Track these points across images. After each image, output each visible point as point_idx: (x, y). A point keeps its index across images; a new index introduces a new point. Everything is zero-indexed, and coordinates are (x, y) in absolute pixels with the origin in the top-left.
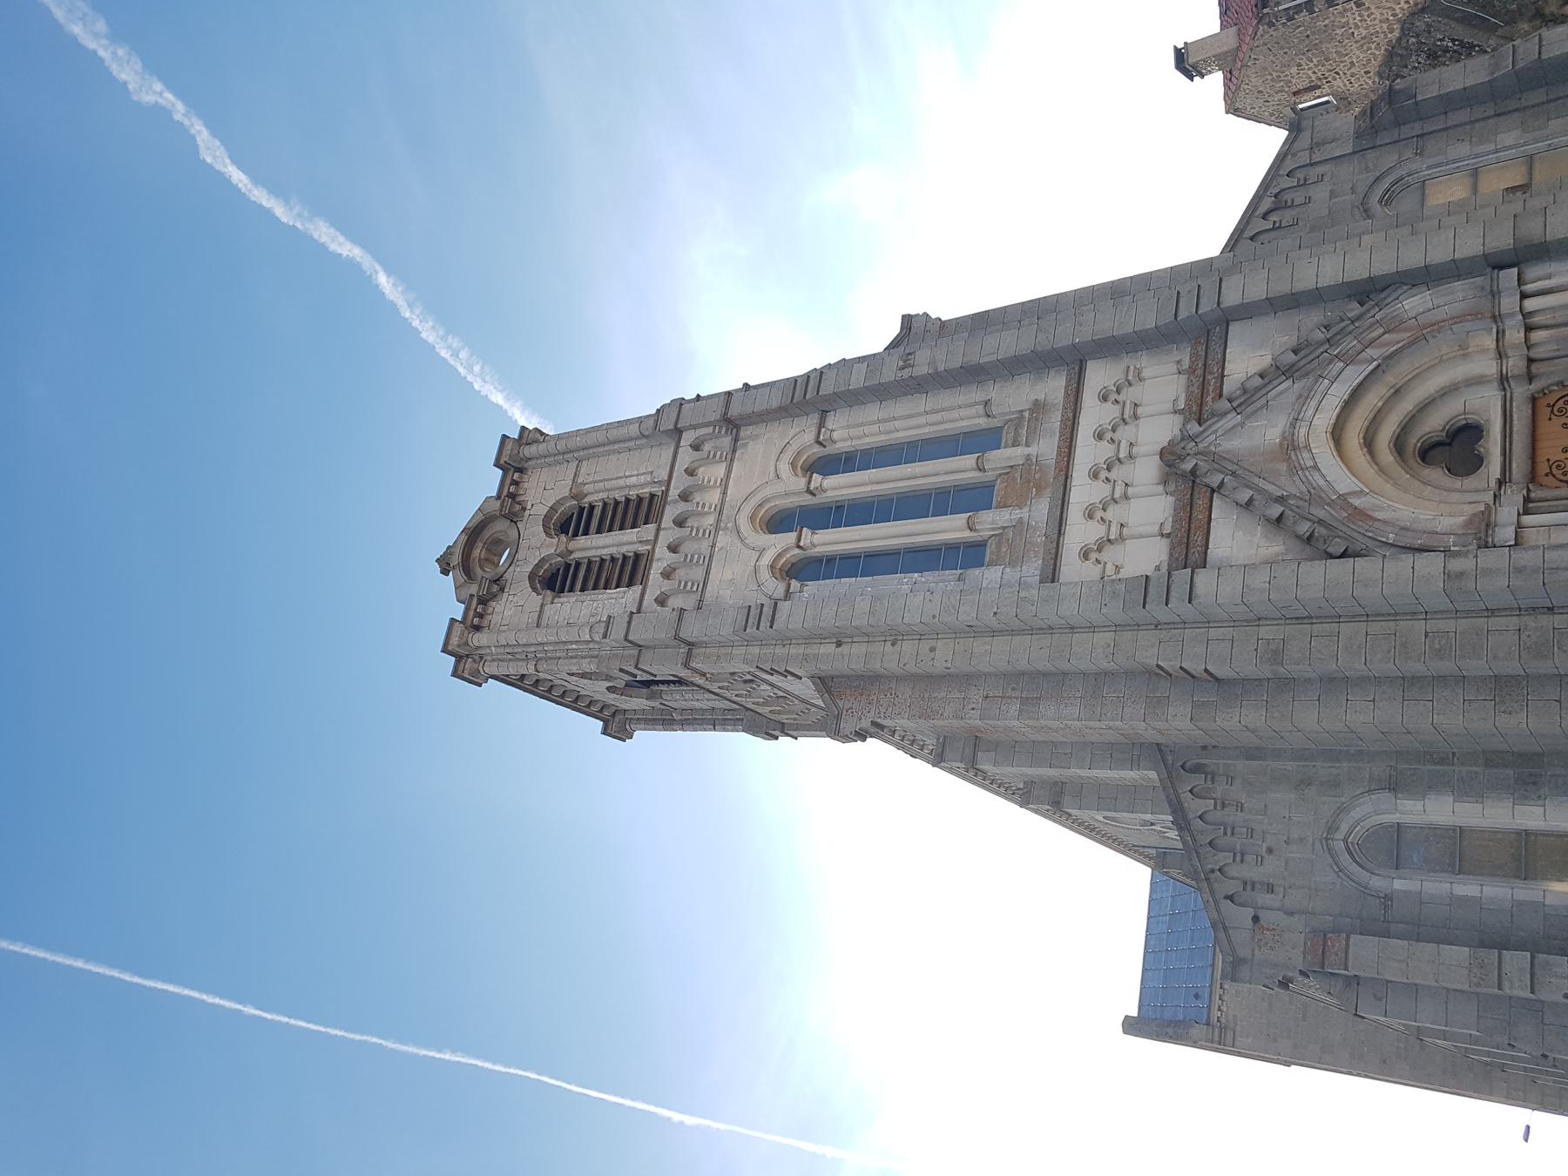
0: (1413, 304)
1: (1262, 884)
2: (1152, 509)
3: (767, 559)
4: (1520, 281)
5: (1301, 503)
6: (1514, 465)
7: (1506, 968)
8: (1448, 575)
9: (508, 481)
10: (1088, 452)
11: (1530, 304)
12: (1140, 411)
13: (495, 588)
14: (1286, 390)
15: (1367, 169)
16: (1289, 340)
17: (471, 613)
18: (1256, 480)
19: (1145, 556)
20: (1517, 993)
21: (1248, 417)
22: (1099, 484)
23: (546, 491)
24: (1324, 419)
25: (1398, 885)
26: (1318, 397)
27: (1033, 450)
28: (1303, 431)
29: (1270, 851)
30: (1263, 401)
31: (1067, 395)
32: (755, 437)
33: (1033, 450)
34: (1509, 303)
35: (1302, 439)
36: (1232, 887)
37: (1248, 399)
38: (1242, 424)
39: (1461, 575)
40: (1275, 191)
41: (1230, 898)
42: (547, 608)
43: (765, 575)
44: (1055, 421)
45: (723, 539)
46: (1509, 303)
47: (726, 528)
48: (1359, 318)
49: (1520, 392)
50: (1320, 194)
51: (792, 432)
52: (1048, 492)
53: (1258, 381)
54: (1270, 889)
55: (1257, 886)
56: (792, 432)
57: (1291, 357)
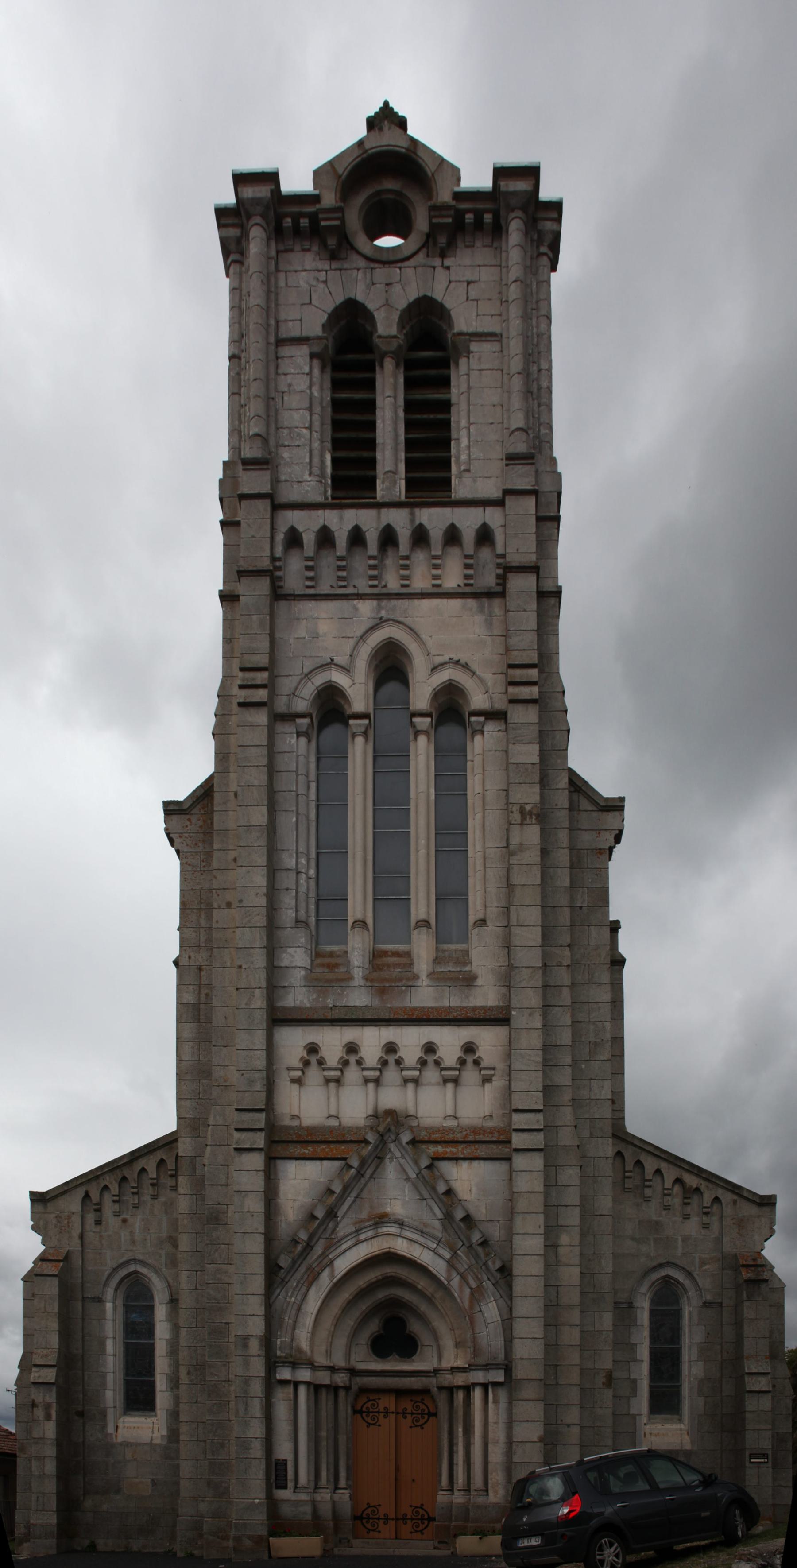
0: (491, 1310)
1: (101, 1216)
2: (354, 1106)
3: (339, 678)
4: (496, 1384)
5: (329, 1231)
6: (374, 1378)
7: (46, 1370)
8: (245, 1340)
9: (480, 206)
10: (410, 1040)
11: (477, 1393)
12: (332, 1085)
13: (332, 242)
14: (434, 1214)
15: (703, 1263)
16: (480, 1212)
17: (295, 209)
18: (354, 1194)
19: (307, 1105)
20: (33, 1375)
21: (414, 1185)
22: (418, 1053)
23: (467, 289)
24: (401, 1247)
25: (109, 1306)
26: (421, 1240)
27: (424, 981)
28: (392, 1230)
29: (124, 1221)
30: (426, 1195)
31: (484, 1009)
32: (489, 624)
33: (424, 981)
34: (479, 1376)
35: (385, 1230)
36: (95, 1195)
37: (428, 1181)
38: (408, 1179)
39: (246, 1346)
40: (703, 1188)
41: (87, 1196)
42: (305, 350)
43: (319, 680)
44: (452, 1000)
45: (366, 608)
46: (479, 1376)
47: (379, 608)
48: (487, 1268)
49: (432, 1382)
50: (692, 1227)
51: (488, 676)
52: (376, 1002)
53: (442, 1188)
54: (98, 1222)
55: (98, 1213)
56: (488, 676)
57: (459, 1214)
